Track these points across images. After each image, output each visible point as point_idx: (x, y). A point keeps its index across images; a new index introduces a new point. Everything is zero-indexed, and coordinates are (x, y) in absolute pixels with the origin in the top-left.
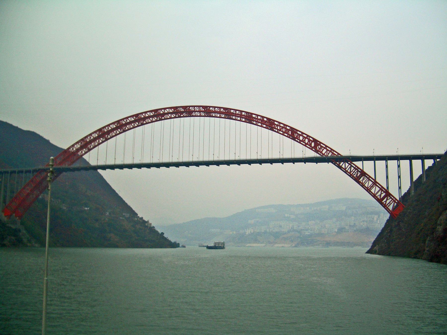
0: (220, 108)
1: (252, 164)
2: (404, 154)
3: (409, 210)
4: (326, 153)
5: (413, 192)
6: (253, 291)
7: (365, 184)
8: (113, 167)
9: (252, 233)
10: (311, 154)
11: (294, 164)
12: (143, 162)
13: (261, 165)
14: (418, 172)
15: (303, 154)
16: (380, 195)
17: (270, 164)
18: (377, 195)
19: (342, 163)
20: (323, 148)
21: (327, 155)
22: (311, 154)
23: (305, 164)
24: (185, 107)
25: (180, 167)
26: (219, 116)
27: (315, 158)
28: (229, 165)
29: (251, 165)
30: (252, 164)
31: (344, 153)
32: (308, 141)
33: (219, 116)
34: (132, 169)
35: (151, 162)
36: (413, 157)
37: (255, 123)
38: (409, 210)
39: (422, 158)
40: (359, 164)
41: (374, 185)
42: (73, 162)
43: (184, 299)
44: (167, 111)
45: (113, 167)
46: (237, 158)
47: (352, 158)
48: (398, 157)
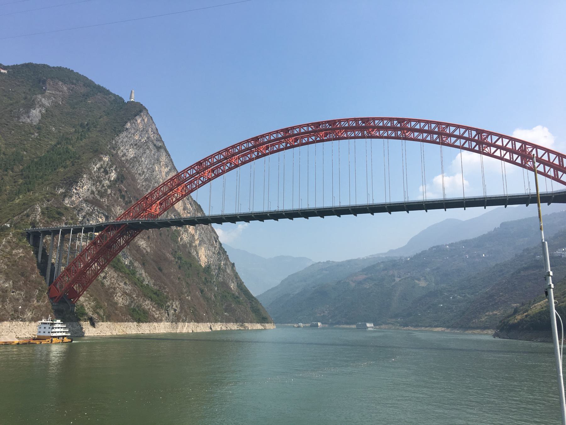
0: (356, 120)
2: (401, 201)
6: (21, 372)
8: (233, 219)
11: (391, 214)
12: (302, 208)
13: (308, 219)
17: (370, 214)
23: (391, 214)
24: (334, 122)
25: (236, 222)
26: (209, 164)
28: (307, 217)
29: (340, 217)
30: (250, 221)
33: (209, 164)
35: (406, 200)
44: (245, 147)
45: (233, 219)
46: (337, 204)
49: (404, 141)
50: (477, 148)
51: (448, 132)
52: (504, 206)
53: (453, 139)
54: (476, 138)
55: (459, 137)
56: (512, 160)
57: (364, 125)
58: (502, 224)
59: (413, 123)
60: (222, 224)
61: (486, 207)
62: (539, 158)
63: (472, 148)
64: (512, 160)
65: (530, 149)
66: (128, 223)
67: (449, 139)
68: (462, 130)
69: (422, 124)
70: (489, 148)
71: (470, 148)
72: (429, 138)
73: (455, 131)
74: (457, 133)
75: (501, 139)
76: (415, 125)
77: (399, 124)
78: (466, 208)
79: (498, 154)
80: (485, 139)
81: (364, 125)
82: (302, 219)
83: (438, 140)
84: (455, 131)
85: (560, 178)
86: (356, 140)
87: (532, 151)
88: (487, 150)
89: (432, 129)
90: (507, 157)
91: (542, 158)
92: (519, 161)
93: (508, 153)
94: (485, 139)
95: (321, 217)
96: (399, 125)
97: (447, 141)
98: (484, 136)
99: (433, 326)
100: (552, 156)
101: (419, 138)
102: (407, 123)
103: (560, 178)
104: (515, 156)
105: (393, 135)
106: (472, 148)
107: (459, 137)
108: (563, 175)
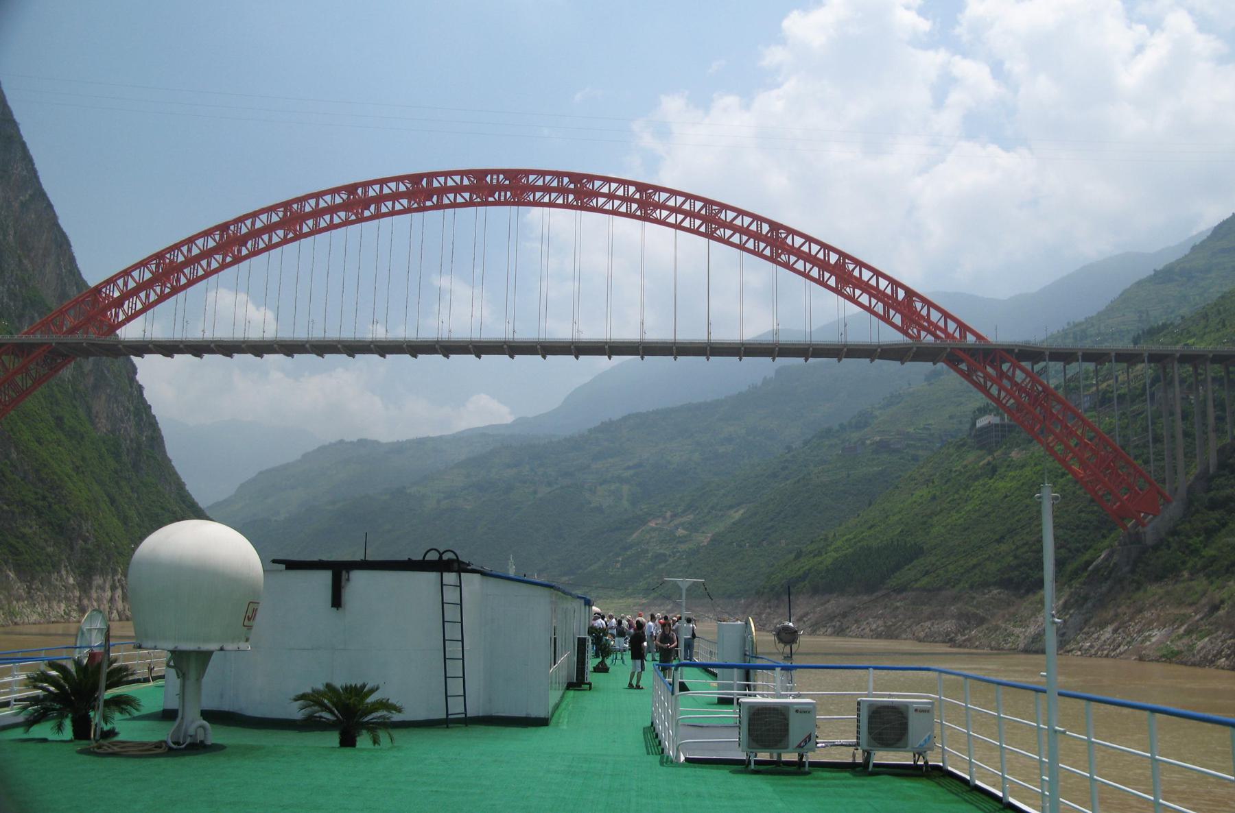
11: (577, 359)
13: (480, 359)
30: (296, 355)
49: (517, 207)
50: (703, 229)
51: (656, 199)
52: (836, 359)
53: (665, 213)
54: (703, 212)
55: (673, 210)
56: (757, 250)
57: (507, 182)
58: (602, 423)
59: (598, 183)
60: (293, 358)
61: (777, 358)
62: (795, 248)
63: (696, 227)
64: (757, 250)
65: (783, 235)
66: (56, 343)
67: (658, 211)
68: (680, 199)
69: (614, 186)
70: (722, 230)
71: (692, 227)
72: (623, 209)
73: (668, 199)
74: (671, 203)
75: (741, 216)
76: (601, 187)
77: (638, 194)
78: (646, 357)
79: (736, 239)
80: (716, 214)
81: (507, 182)
82: (219, 358)
83: (639, 213)
84: (668, 199)
85: (858, 298)
86: (552, 209)
87: (786, 237)
88: (720, 232)
89: (630, 195)
90: (750, 245)
91: (802, 249)
92: (767, 252)
93: (752, 240)
94: (716, 214)
95: (318, 355)
96: (572, 186)
97: (654, 215)
98: (715, 210)
99: (1187, 603)
100: (815, 248)
101: (606, 207)
102: (588, 182)
103: (858, 298)
104: (762, 245)
105: (560, 201)
106: (696, 227)
107: (673, 210)
108: (885, 289)
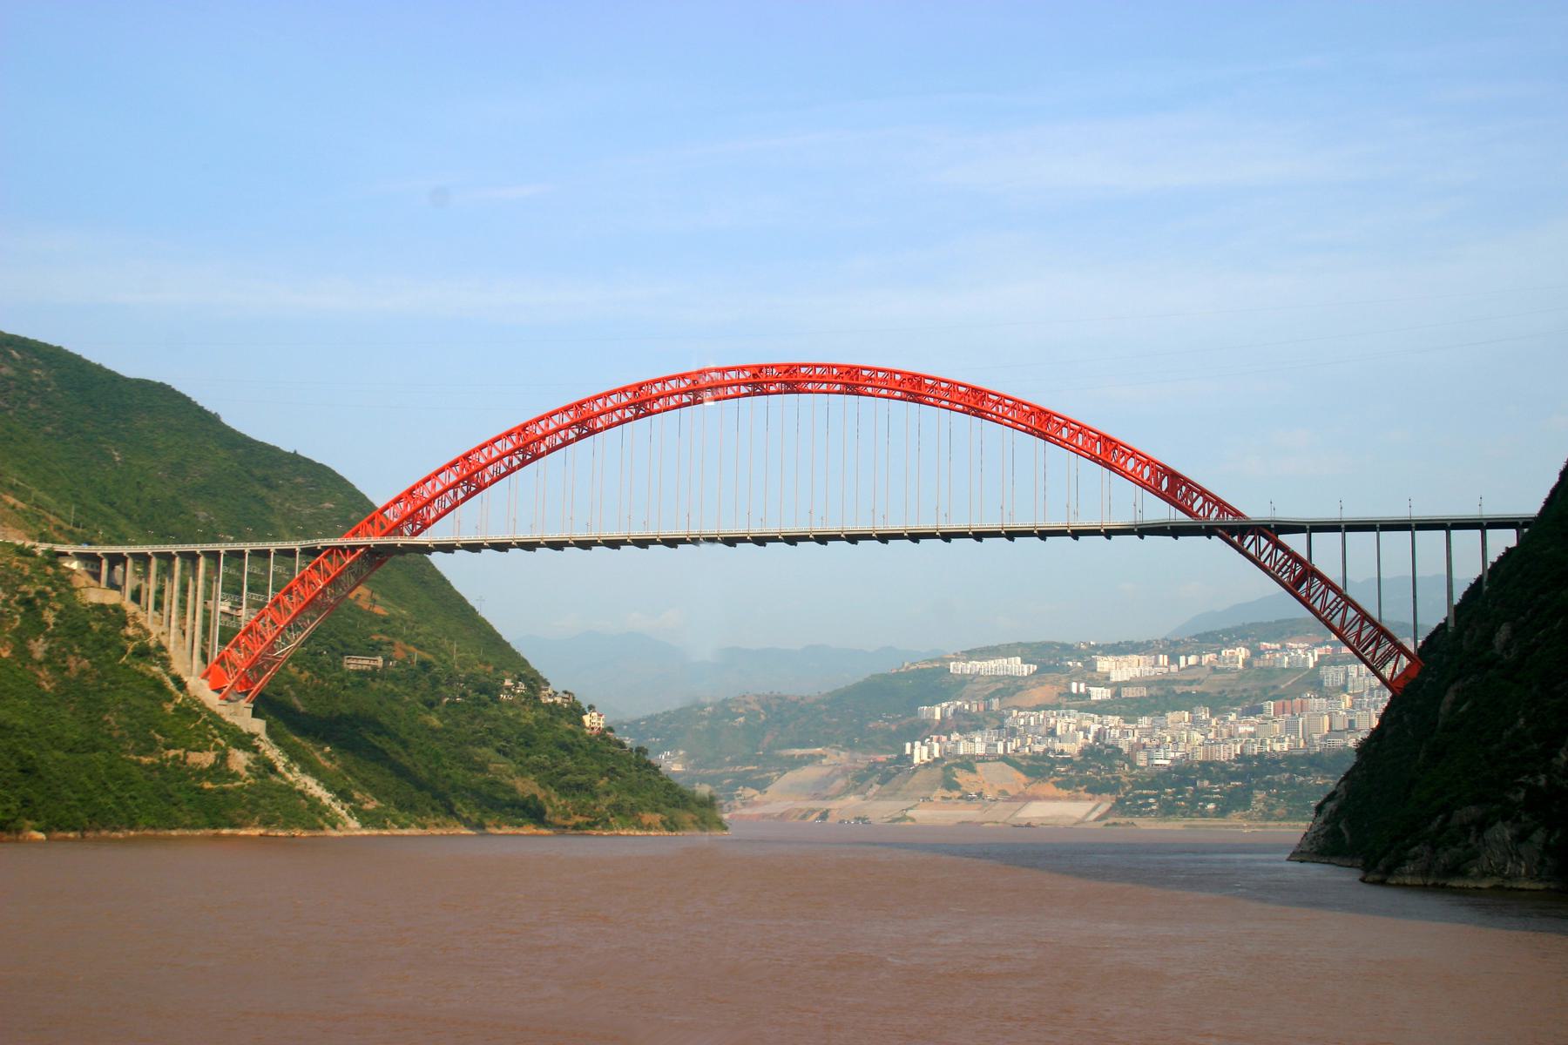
1: (1146, 537)
3: (1430, 679)
4: (1202, 510)
5: (1451, 624)
7: (1336, 598)
9: (936, 760)
10: (1161, 511)
14: (1469, 570)
15: (1136, 511)
16: (1358, 635)
17: (1205, 537)
18: (1372, 628)
19: (1250, 538)
20: (1195, 495)
21: (1206, 514)
22: (1161, 511)
27: (1171, 527)
31: (1255, 511)
32: (1152, 473)
34: (765, 546)
36: (1524, 523)
37: (869, 390)
38: (1430, 679)
39: (1483, 525)
40: (1296, 542)
41: (1161, 656)
42: (425, 526)
43: (1260, 710)
47: (1138, 529)
48: (1410, 525)
